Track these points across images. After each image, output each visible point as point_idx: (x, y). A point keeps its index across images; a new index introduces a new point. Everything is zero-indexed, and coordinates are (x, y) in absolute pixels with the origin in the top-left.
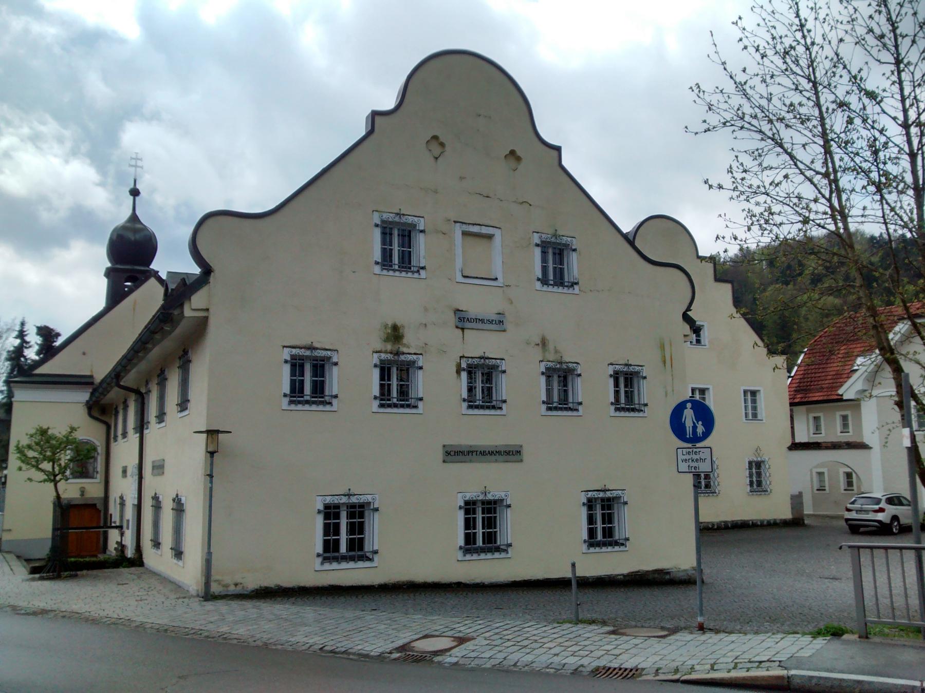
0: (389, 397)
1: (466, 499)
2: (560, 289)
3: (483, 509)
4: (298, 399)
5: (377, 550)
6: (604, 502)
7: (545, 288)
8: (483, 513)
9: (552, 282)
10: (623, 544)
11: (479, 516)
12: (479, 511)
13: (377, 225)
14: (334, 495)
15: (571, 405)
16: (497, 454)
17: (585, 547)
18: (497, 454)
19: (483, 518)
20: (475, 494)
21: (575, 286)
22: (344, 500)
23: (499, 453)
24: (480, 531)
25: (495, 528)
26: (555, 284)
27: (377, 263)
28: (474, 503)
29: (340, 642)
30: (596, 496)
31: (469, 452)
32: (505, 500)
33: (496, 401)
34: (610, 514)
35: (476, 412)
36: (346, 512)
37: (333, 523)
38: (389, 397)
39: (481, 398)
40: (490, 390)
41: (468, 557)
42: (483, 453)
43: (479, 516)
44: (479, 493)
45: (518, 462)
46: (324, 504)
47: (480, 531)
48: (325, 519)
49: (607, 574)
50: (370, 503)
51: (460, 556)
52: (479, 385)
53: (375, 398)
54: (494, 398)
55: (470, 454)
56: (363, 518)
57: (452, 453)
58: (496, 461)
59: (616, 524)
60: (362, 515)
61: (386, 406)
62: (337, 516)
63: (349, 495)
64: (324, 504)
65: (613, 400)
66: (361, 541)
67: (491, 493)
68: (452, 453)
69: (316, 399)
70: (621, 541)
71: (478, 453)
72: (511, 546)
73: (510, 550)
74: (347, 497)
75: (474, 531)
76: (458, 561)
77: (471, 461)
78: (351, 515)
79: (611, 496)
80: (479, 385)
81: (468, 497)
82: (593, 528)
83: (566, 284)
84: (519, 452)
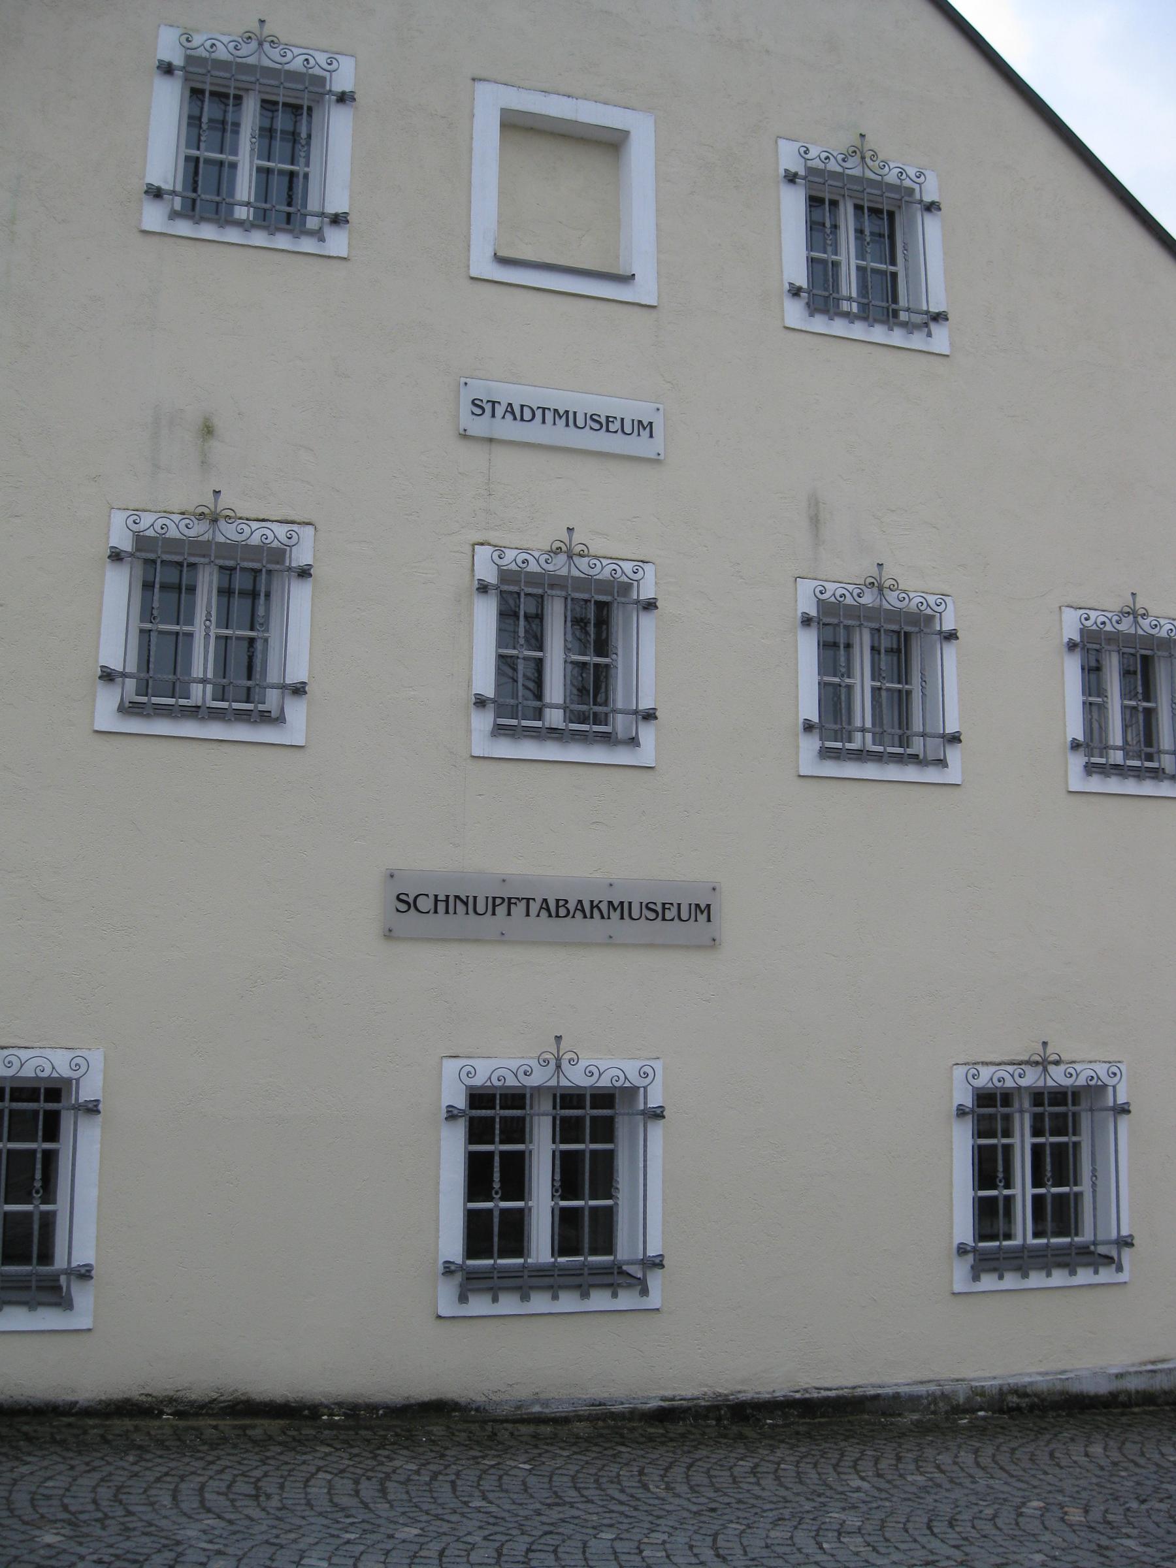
0: (1149, 750)
1: (478, 1081)
2: (878, 334)
3: (1037, 1119)
4: (514, 722)
5: (1131, 1236)
6: (1041, 1104)
7: (819, 324)
8: (1037, 1132)
9: (241, 213)
10: (1108, 1260)
11: (1022, 1142)
12: (1022, 1125)
13: (167, 69)
14: (999, 1064)
15: (917, 746)
16: (615, 916)
17: (961, 1269)
18: (615, 916)
19: (1037, 1151)
20: (514, 1064)
21: (933, 327)
22: (1031, 1078)
23: (621, 909)
24: (1023, 1190)
25: (1008, 1186)
26: (865, 315)
27: (795, 292)
28: (516, 1099)
29: (1015, 1553)
30: (1010, 1083)
31: (494, 904)
32: (1110, 1089)
33: (924, 735)
34: (1060, 1151)
35: (851, 770)
36: (550, 1118)
37: (502, 1153)
38: (1149, 750)
39: (868, 724)
40: (903, 700)
41: (479, 1305)
42: (555, 909)
43: (1022, 1142)
44: (533, 1063)
45: (699, 947)
46: (469, 1088)
47: (1023, 1190)
48: (980, 1133)
49: (926, 1375)
50: (635, 1089)
51: (446, 1299)
52: (862, 683)
53: (808, 727)
54: (917, 726)
55: (502, 910)
56: (522, 1141)
57: (425, 904)
58: (610, 942)
59: (1085, 1187)
60: (605, 1130)
61: (885, 758)
62: (517, 1131)
63: (1043, 1064)
64: (469, 1088)
65: (1076, 731)
66: (605, 1222)
67: (583, 1064)
68: (425, 904)
69: (525, 723)
70: (1102, 1250)
71: (534, 907)
72: (661, 1266)
73: (655, 1281)
74: (1040, 1068)
75: (1006, 1192)
76: (439, 1317)
77: (502, 938)
78: (567, 1130)
79: (1067, 1082)
80: (862, 683)
81: (485, 1073)
82: (1066, 1195)
83: (903, 316)
84: (704, 911)
